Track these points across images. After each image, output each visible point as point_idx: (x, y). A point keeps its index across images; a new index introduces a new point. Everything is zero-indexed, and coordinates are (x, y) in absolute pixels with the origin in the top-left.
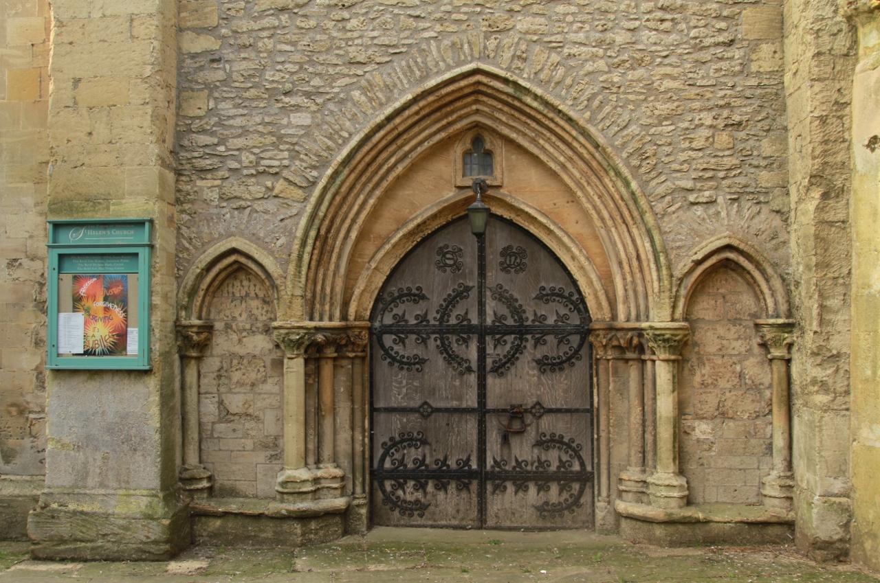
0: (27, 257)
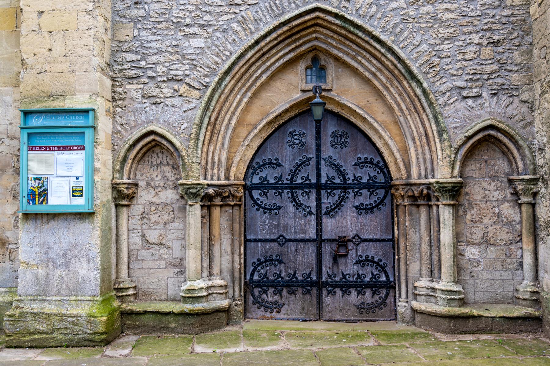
0: (8, 137)
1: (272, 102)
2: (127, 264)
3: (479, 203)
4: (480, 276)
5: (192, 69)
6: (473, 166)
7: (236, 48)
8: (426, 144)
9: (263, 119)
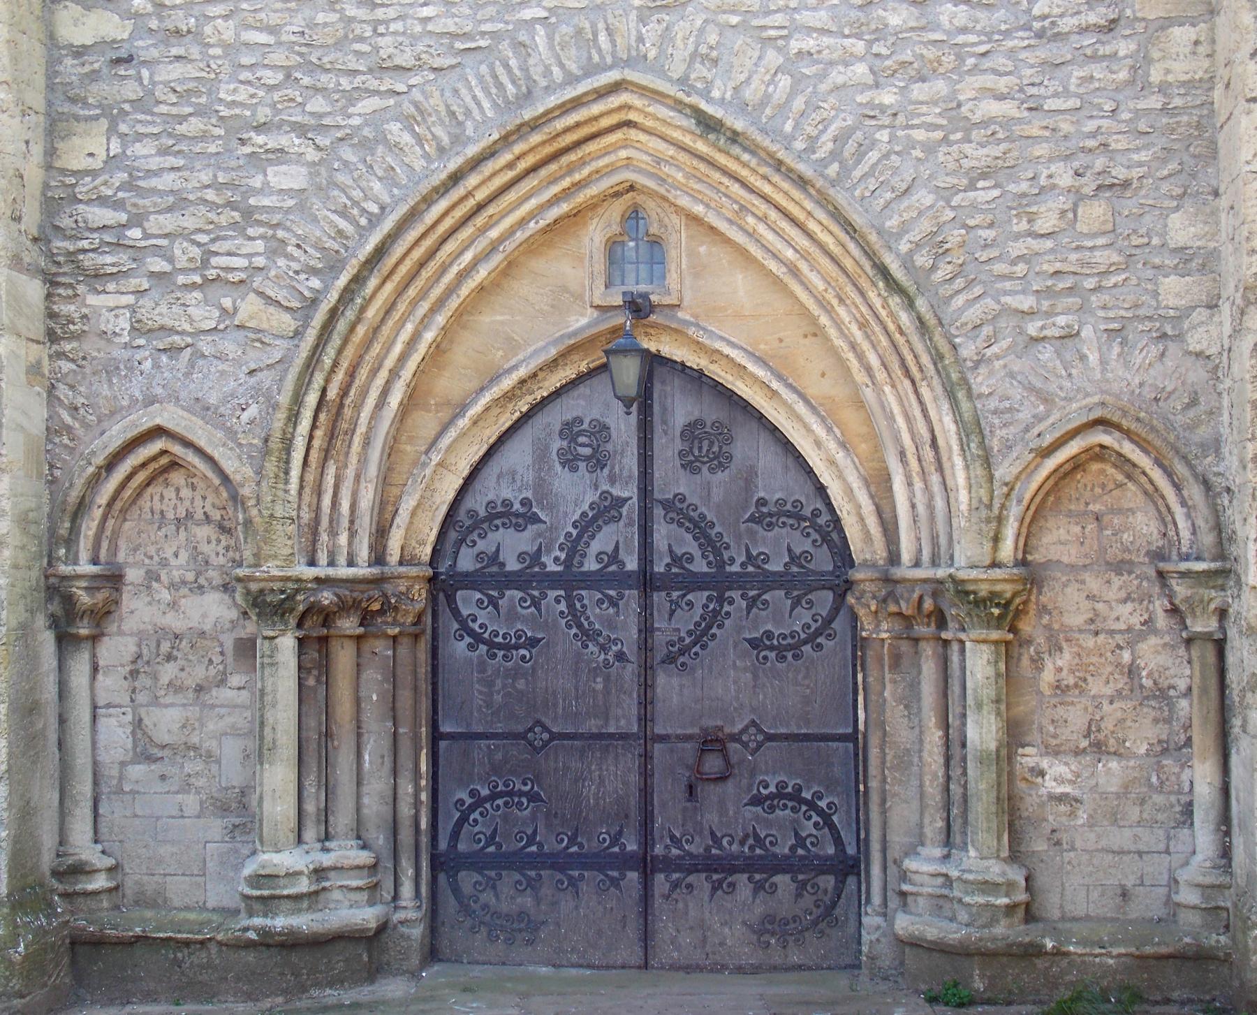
1: (509, 339)
2: (90, 804)
3: (1077, 635)
4: (1078, 844)
5: (274, 252)
6: (1062, 531)
7: (396, 191)
8: (933, 469)
9: (482, 389)
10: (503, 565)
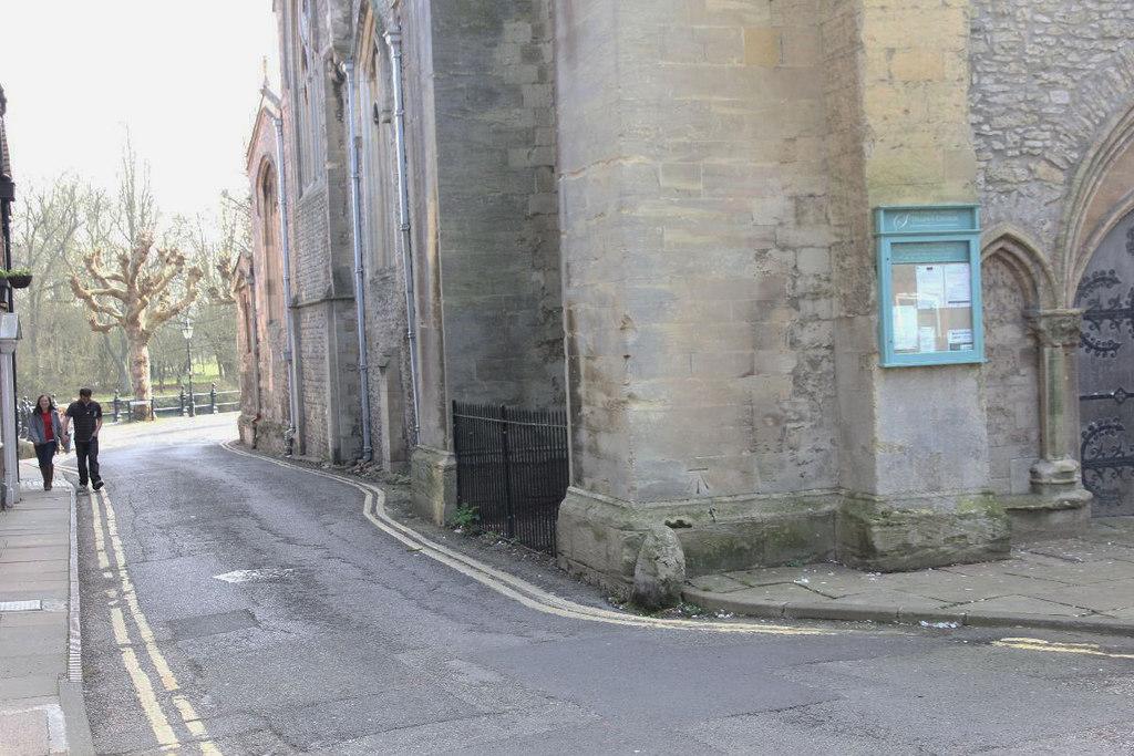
0: (778, 247)
7: (1113, 105)
10: (1101, 307)
